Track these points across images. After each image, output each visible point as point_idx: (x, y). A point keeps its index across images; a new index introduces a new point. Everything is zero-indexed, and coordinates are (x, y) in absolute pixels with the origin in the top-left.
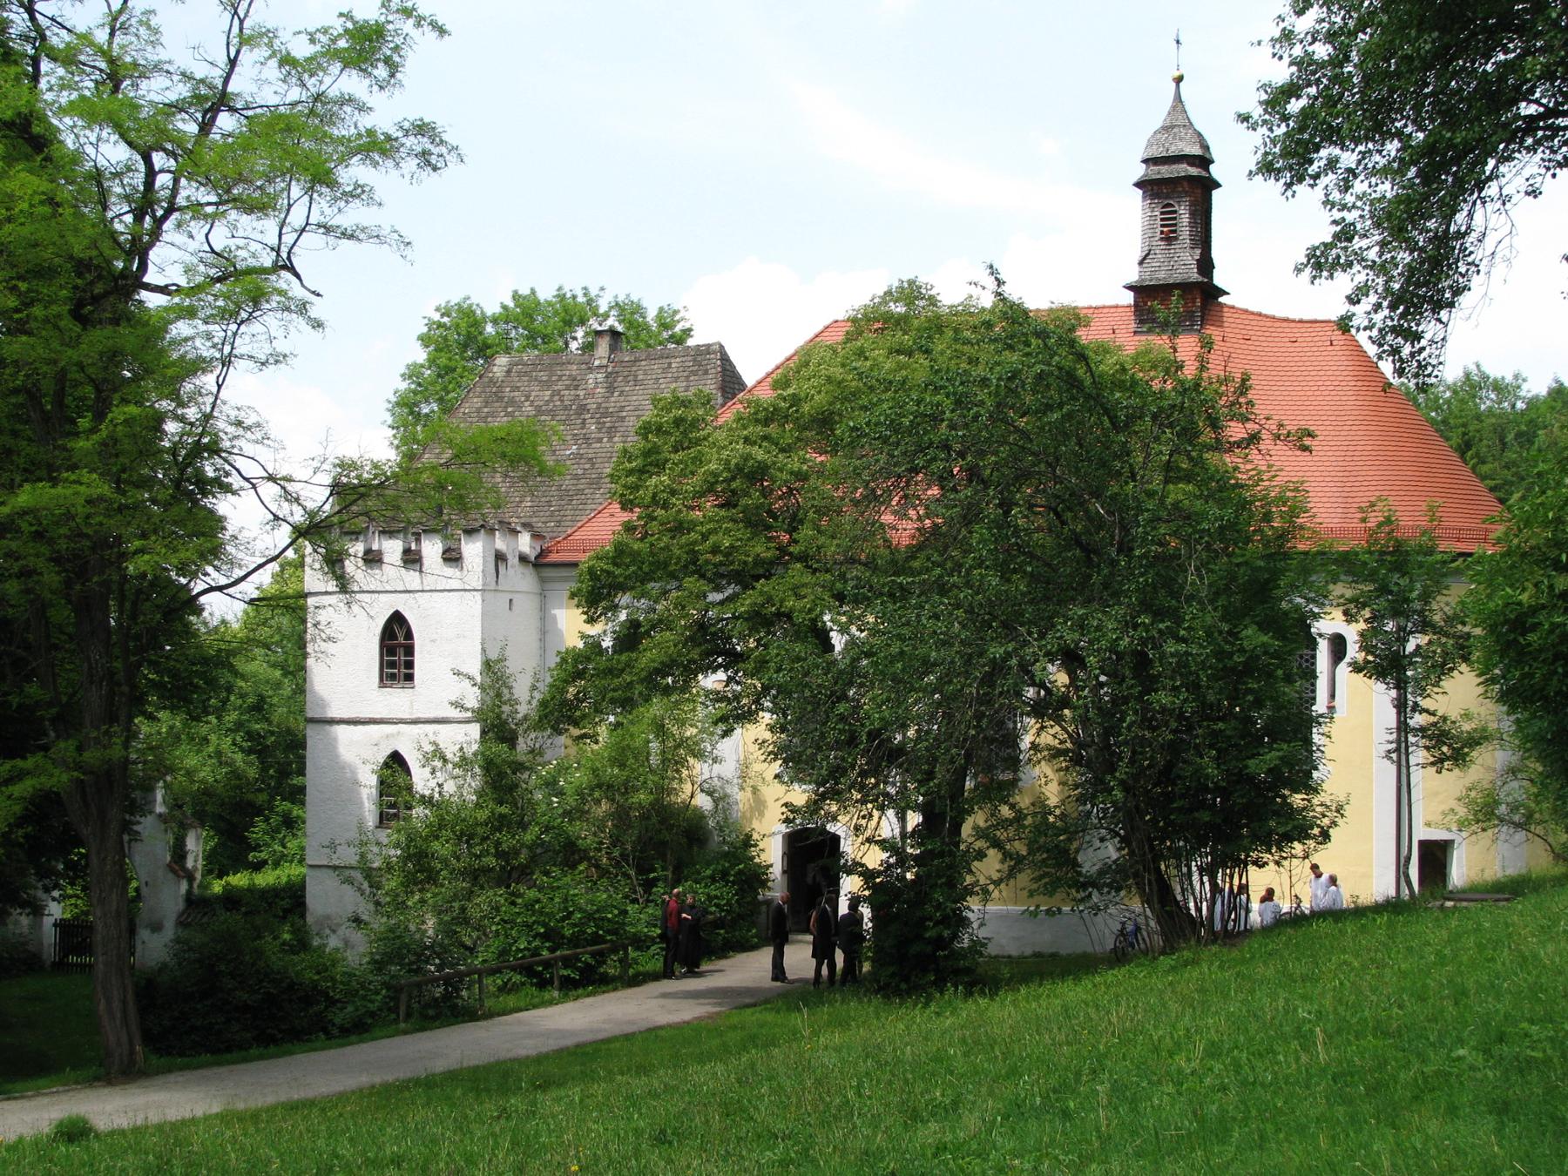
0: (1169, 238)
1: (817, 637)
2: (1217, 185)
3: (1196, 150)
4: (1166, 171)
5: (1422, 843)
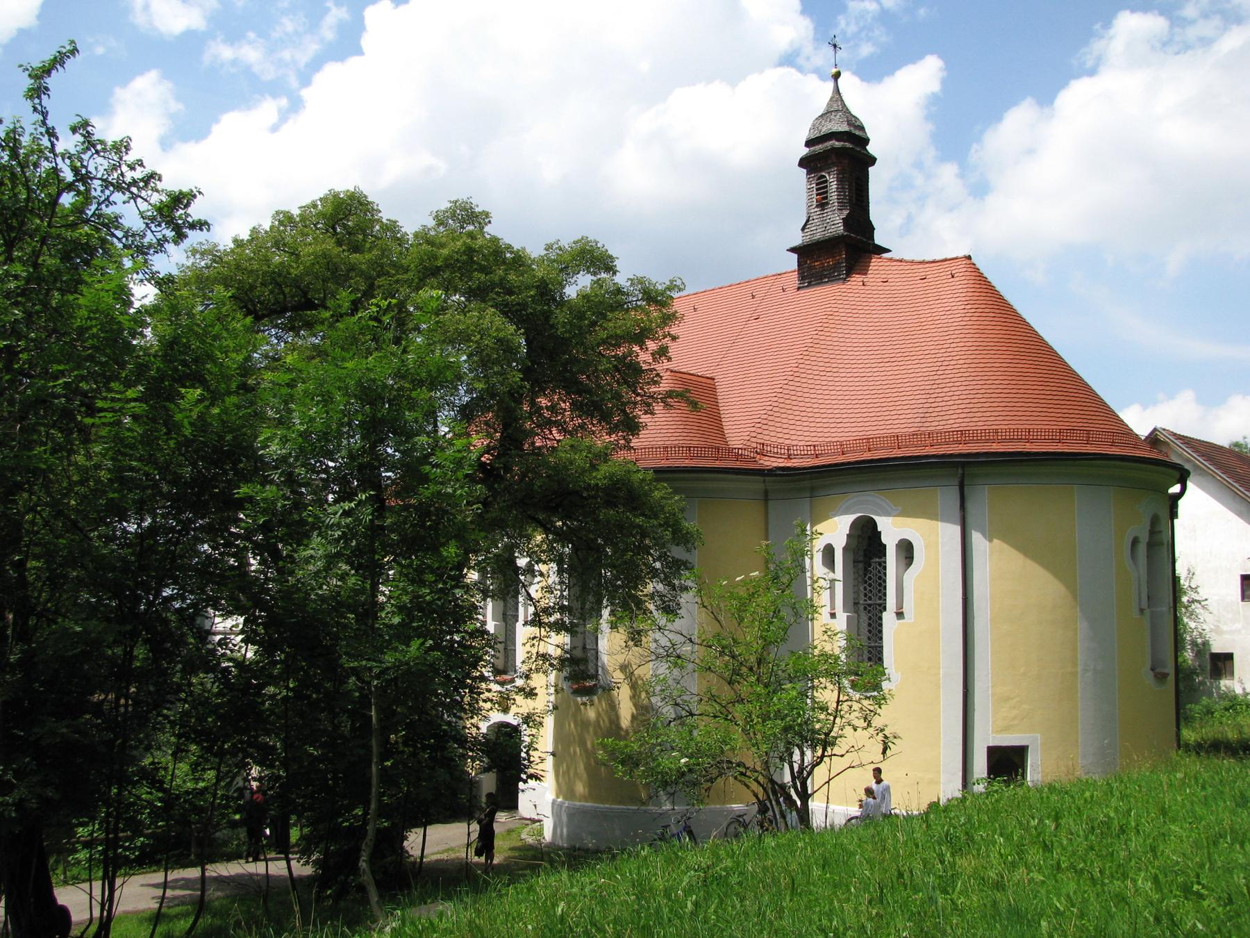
0: (822, 204)
1: (534, 869)
2: (872, 161)
3: (844, 128)
4: (818, 148)
5: (993, 752)
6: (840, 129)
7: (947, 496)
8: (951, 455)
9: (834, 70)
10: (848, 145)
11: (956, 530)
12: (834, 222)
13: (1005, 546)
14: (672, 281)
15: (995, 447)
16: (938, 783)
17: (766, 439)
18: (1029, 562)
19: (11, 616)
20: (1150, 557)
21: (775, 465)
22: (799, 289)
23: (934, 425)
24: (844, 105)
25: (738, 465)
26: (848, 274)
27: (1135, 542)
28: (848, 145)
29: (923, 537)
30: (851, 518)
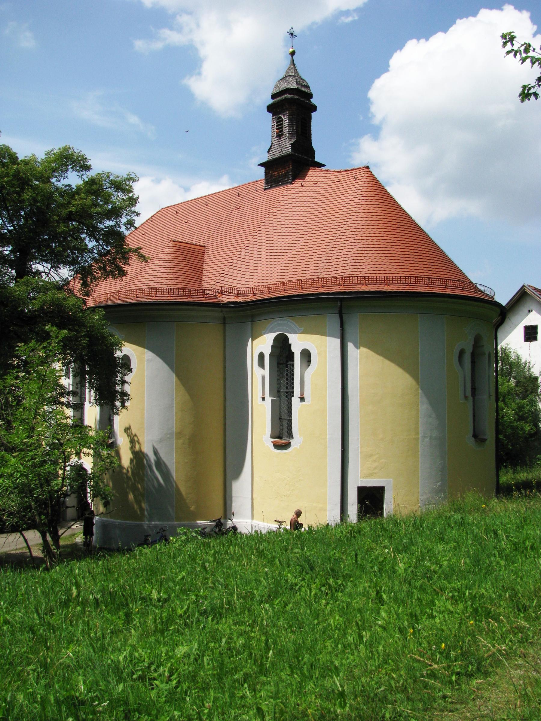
2: (314, 108)
3: (294, 86)
6: (291, 87)
7: (332, 321)
8: (334, 293)
9: (291, 50)
10: (296, 97)
11: (338, 341)
12: (286, 146)
13: (371, 353)
14: (129, 175)
15: (364, 288)
16: (325, 510)
17: (225, 284)
18: (387, 362)
19: (140, 486)
20: (473, 362)
21: (228, 300)
22: (265, 189)
23: (329, 273)
24: (296, 71)
25: (204, 300)
26: (294, 180)
27: (462, 353)
28: (296, 97)
29: (317, 347)
30: (274, 335)
